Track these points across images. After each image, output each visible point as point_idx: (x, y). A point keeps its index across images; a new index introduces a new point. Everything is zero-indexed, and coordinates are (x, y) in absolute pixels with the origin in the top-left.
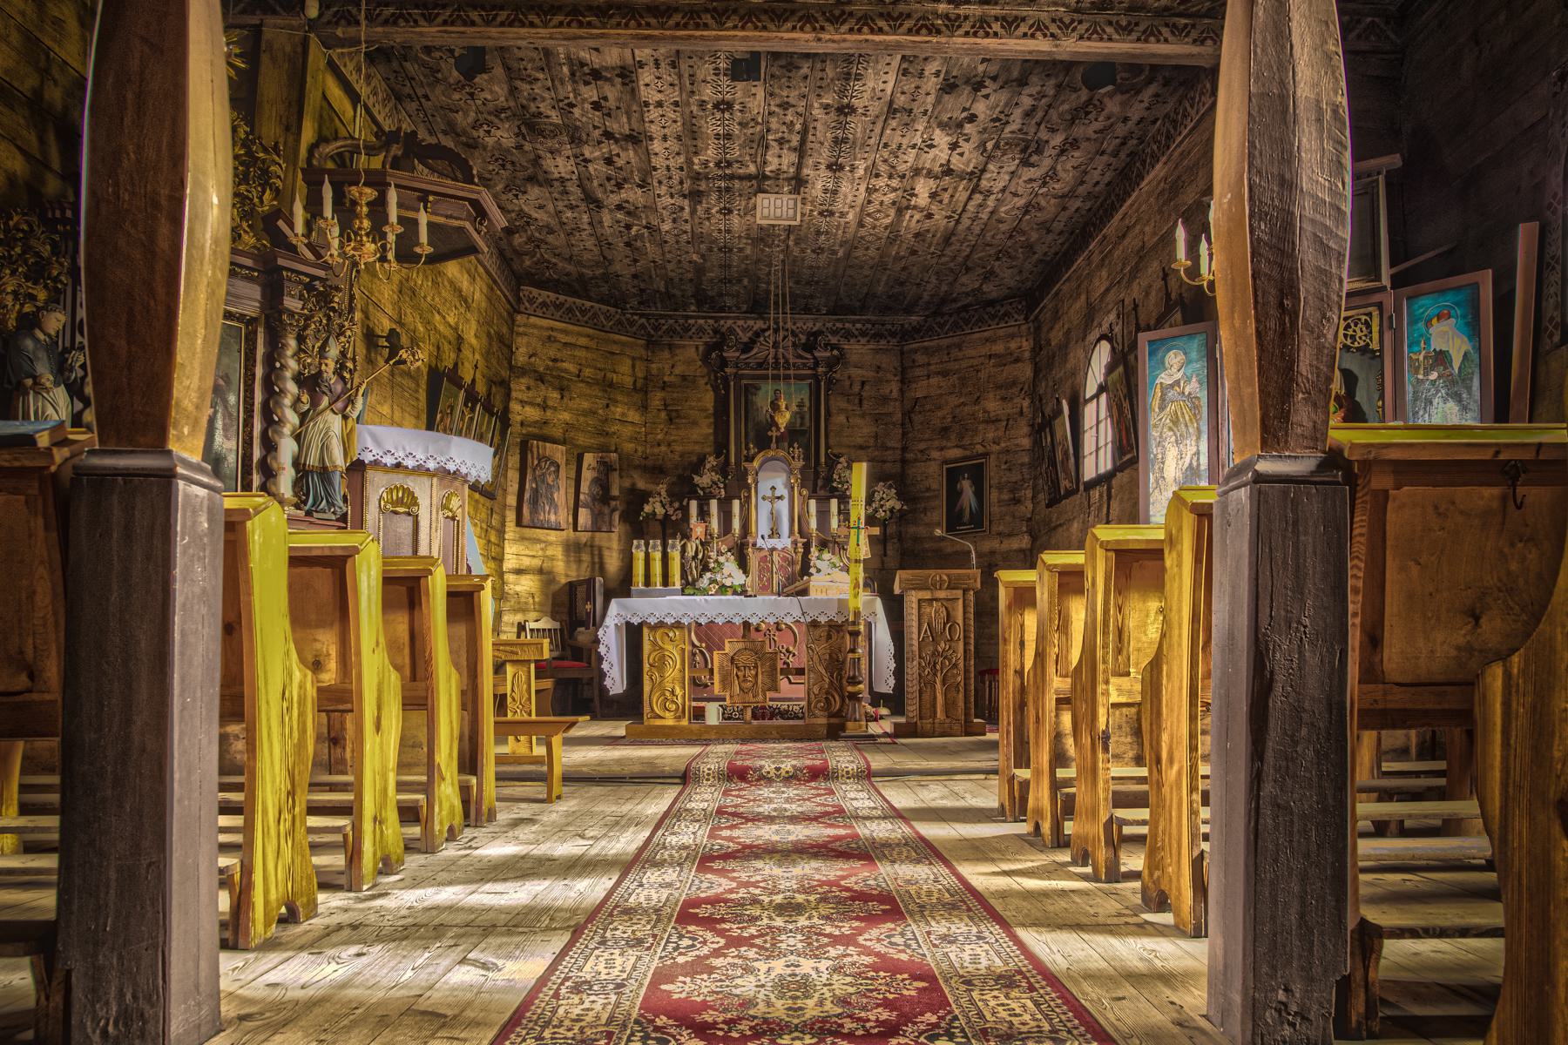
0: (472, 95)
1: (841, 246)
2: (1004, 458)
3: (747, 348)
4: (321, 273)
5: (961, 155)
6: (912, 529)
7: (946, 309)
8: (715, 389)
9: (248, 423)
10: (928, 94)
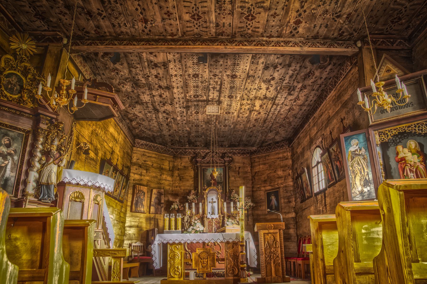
0: (117, 73)
1: (232, 124)
2: (284, 189)
3: (204, 158)
4: (55, 116)
5: (270, 92)
6: (256, 212)
7: (264, 144)
8: (194, 170)
9: (21, 167)
10: (260, 70)
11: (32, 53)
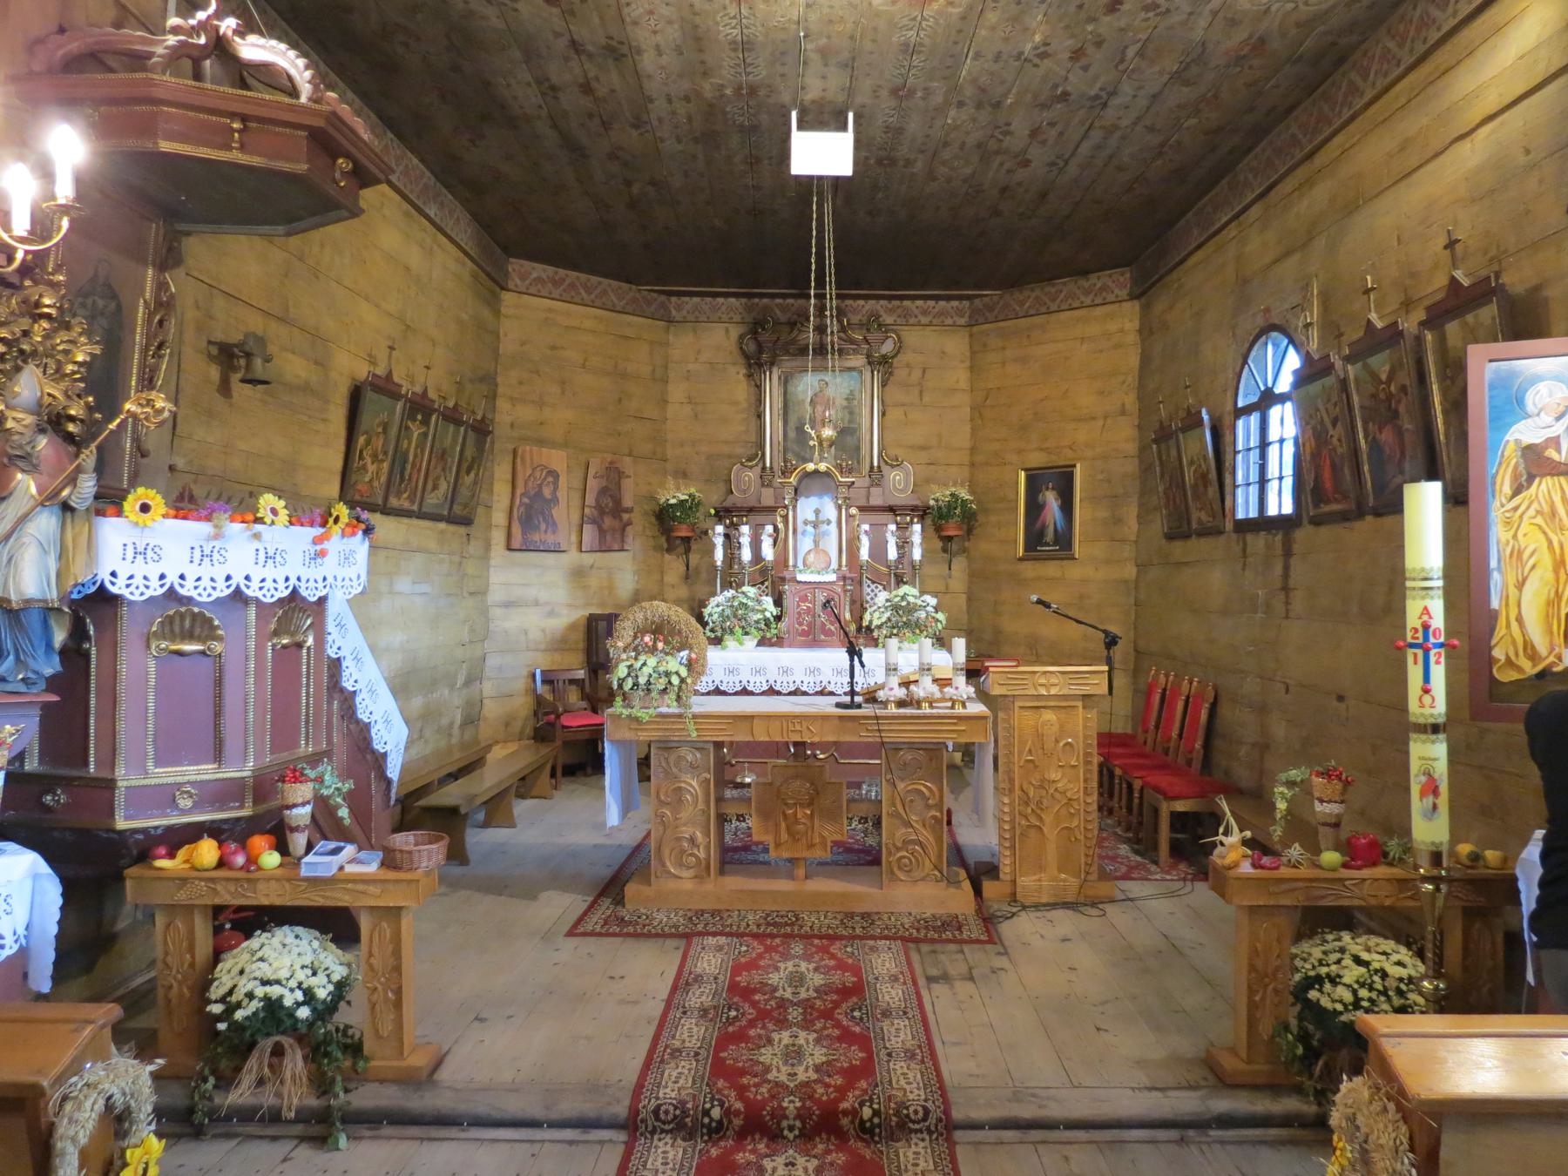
5: (1085, 68)
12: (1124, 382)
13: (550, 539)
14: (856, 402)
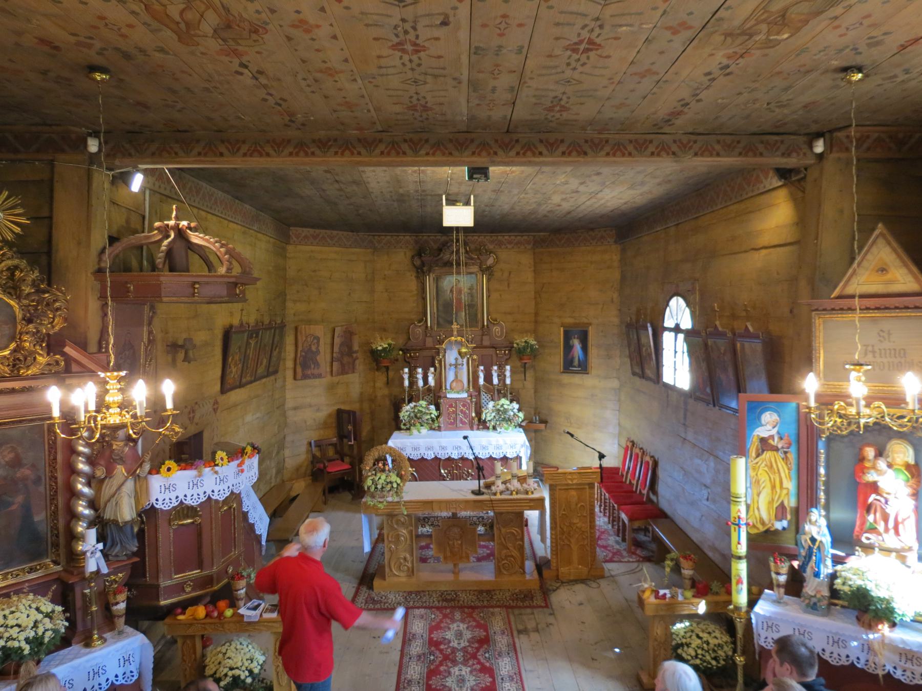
11: (17, 230)
12: (612, 287)
13: (316, 372)
14: (474, 291)
